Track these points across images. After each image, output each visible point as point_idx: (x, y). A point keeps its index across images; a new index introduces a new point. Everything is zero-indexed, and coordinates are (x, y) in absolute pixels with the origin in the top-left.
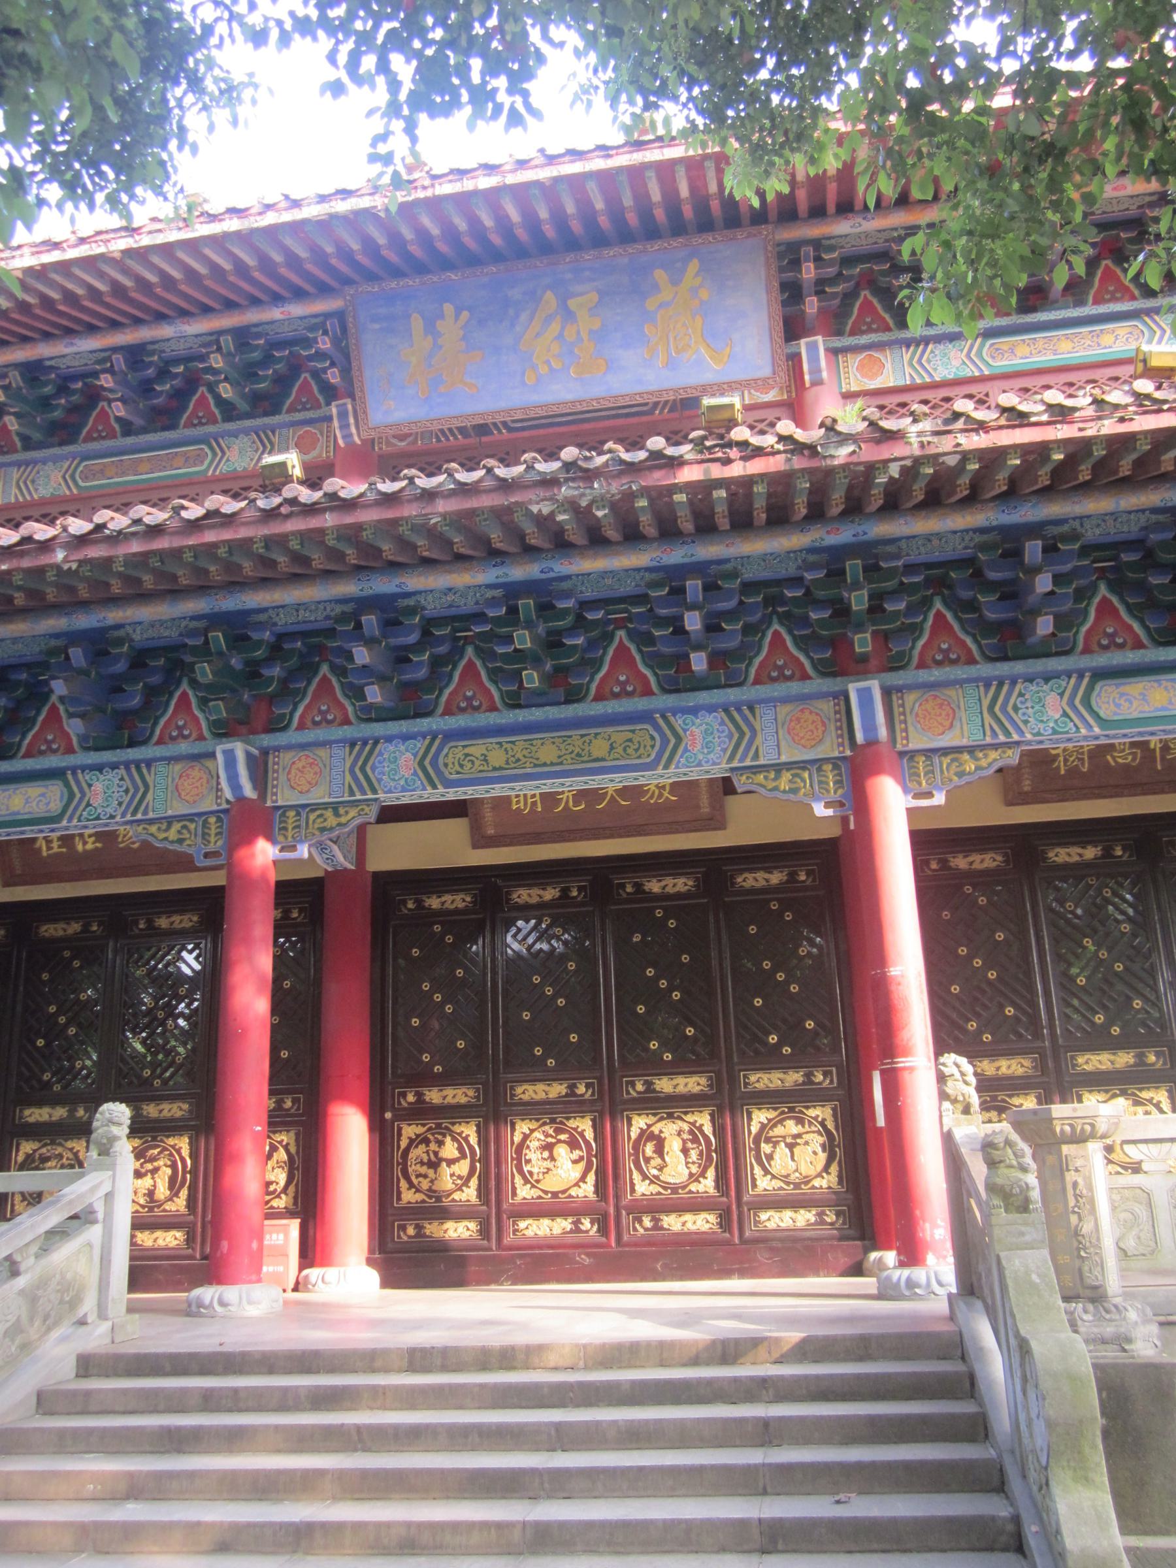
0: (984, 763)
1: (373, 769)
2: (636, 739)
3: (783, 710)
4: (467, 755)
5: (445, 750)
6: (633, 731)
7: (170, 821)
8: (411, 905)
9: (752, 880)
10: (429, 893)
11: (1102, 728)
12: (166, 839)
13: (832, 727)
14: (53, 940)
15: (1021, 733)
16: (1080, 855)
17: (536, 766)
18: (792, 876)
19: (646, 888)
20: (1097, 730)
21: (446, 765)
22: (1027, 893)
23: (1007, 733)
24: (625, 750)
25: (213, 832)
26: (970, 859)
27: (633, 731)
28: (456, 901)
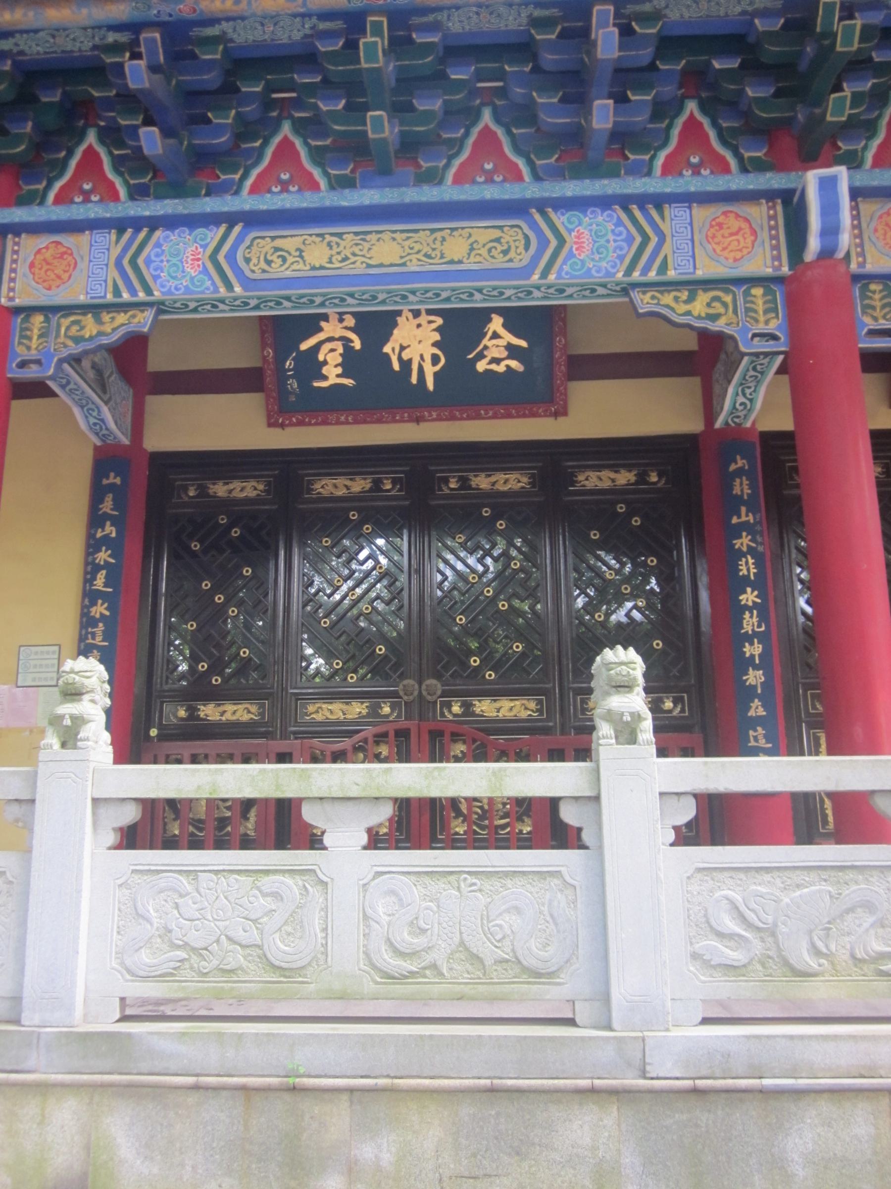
0: (108, 328)
1: (148, 262)
2: (506, 238)
3: (702, 214)
4: (277, 249)
5: (247, 242)
6: (500, 228)
7: (695, 286)
9: (594, 480)
10: (215, 478)
11: (245, 288)
12: (688, 313)
13: (764, 235)
15: (149, 291)
16: (613, 480)
18: (377, 485)
20: (238, 289)
21: (248, 260)
23: (133, 292)
24: (490, 251)
25: (760, 308)
26: (493, 479)
27: (500, 228)
28: (247, 489)
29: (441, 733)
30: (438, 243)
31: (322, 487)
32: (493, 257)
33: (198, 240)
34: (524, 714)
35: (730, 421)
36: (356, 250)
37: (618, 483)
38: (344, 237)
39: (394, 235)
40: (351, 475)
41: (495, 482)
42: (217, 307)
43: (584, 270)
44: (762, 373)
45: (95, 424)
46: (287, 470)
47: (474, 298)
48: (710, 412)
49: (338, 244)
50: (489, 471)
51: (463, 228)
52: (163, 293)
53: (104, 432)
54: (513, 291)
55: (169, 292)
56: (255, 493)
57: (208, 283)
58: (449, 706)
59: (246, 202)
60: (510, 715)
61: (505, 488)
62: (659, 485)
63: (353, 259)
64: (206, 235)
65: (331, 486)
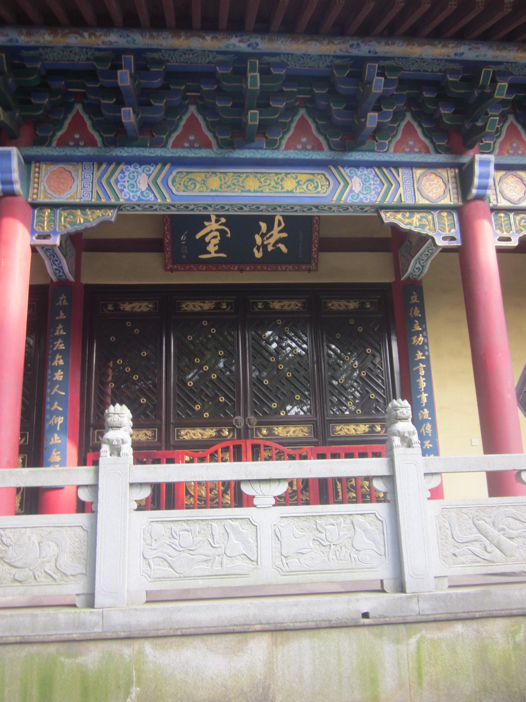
4: (190, 179)
6: (313, 174)
8: (110, 308)
14: (193, 313)
16: (201, 307)
17: (242, 191)
18: (218, 306)
19: (271, 306)
22: (320, 334)
29: (258, 446)
30: (279, 180)
31: (187, 306)
32: (309, 190)
33: (145, 171)
34: (301, 435)
35: (411, 276)
36: (235, 181)
37: (349, 308)
38: (228, 174)
39: (256, 175)
40: (203, 300)
41: (284, 305)
42: (207, 208)
43: (359, 199)
44: (432, 254)
45: (56, 269)
46: (168, 297)
47: (349, 210)
48: (398, 271)
49: (224, 178)
50: (280, 299)
51: (293, 173)
52: (125, 200)
53: (61, 274)
54: (264, 207)
55: (129, 199)
56: (148, 309)
57: (151, 196)
58: (260, 431)
59: (168, 152)
60: (293, 435)
61: (139, 310)
62: (371, 309)
63: (233, 187)
64: (150, 170)
65: (191, 306)
